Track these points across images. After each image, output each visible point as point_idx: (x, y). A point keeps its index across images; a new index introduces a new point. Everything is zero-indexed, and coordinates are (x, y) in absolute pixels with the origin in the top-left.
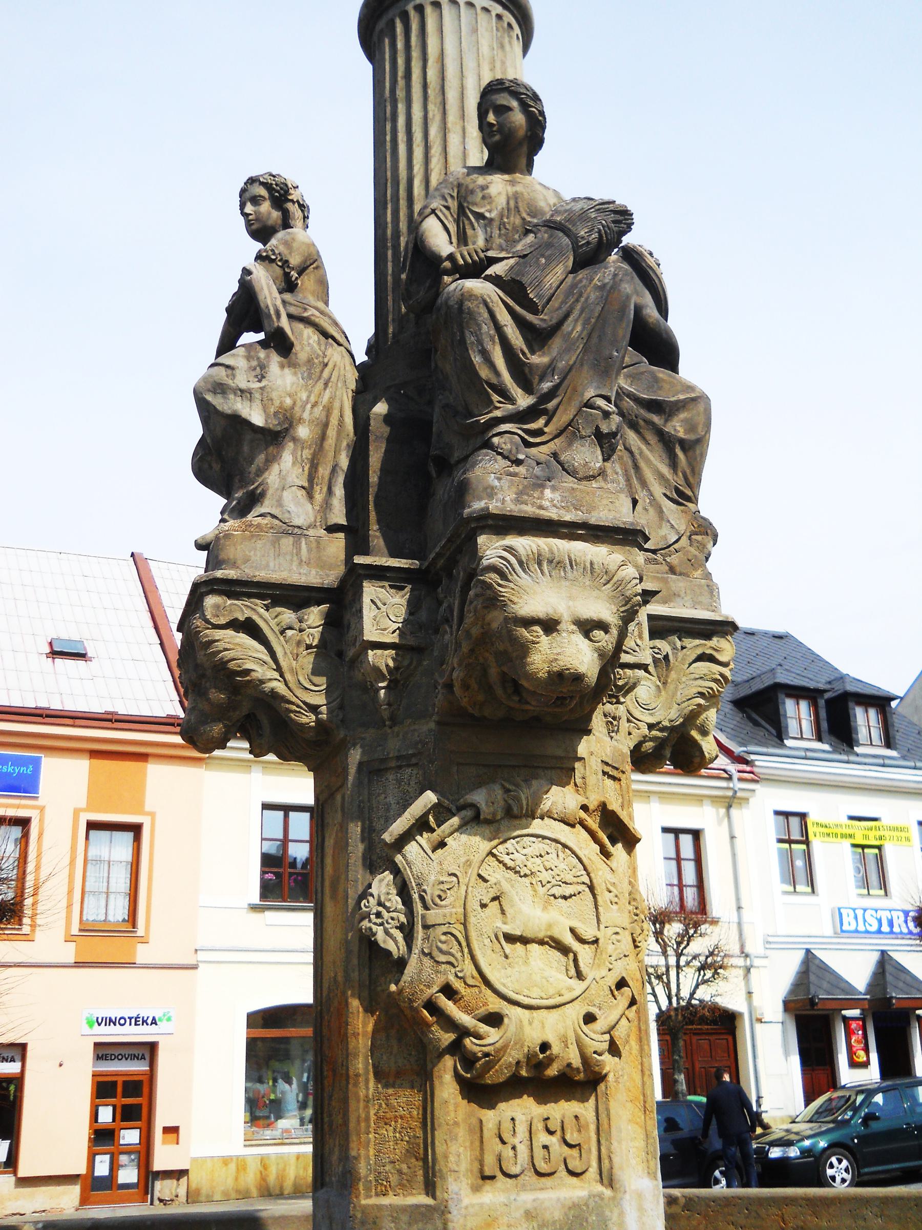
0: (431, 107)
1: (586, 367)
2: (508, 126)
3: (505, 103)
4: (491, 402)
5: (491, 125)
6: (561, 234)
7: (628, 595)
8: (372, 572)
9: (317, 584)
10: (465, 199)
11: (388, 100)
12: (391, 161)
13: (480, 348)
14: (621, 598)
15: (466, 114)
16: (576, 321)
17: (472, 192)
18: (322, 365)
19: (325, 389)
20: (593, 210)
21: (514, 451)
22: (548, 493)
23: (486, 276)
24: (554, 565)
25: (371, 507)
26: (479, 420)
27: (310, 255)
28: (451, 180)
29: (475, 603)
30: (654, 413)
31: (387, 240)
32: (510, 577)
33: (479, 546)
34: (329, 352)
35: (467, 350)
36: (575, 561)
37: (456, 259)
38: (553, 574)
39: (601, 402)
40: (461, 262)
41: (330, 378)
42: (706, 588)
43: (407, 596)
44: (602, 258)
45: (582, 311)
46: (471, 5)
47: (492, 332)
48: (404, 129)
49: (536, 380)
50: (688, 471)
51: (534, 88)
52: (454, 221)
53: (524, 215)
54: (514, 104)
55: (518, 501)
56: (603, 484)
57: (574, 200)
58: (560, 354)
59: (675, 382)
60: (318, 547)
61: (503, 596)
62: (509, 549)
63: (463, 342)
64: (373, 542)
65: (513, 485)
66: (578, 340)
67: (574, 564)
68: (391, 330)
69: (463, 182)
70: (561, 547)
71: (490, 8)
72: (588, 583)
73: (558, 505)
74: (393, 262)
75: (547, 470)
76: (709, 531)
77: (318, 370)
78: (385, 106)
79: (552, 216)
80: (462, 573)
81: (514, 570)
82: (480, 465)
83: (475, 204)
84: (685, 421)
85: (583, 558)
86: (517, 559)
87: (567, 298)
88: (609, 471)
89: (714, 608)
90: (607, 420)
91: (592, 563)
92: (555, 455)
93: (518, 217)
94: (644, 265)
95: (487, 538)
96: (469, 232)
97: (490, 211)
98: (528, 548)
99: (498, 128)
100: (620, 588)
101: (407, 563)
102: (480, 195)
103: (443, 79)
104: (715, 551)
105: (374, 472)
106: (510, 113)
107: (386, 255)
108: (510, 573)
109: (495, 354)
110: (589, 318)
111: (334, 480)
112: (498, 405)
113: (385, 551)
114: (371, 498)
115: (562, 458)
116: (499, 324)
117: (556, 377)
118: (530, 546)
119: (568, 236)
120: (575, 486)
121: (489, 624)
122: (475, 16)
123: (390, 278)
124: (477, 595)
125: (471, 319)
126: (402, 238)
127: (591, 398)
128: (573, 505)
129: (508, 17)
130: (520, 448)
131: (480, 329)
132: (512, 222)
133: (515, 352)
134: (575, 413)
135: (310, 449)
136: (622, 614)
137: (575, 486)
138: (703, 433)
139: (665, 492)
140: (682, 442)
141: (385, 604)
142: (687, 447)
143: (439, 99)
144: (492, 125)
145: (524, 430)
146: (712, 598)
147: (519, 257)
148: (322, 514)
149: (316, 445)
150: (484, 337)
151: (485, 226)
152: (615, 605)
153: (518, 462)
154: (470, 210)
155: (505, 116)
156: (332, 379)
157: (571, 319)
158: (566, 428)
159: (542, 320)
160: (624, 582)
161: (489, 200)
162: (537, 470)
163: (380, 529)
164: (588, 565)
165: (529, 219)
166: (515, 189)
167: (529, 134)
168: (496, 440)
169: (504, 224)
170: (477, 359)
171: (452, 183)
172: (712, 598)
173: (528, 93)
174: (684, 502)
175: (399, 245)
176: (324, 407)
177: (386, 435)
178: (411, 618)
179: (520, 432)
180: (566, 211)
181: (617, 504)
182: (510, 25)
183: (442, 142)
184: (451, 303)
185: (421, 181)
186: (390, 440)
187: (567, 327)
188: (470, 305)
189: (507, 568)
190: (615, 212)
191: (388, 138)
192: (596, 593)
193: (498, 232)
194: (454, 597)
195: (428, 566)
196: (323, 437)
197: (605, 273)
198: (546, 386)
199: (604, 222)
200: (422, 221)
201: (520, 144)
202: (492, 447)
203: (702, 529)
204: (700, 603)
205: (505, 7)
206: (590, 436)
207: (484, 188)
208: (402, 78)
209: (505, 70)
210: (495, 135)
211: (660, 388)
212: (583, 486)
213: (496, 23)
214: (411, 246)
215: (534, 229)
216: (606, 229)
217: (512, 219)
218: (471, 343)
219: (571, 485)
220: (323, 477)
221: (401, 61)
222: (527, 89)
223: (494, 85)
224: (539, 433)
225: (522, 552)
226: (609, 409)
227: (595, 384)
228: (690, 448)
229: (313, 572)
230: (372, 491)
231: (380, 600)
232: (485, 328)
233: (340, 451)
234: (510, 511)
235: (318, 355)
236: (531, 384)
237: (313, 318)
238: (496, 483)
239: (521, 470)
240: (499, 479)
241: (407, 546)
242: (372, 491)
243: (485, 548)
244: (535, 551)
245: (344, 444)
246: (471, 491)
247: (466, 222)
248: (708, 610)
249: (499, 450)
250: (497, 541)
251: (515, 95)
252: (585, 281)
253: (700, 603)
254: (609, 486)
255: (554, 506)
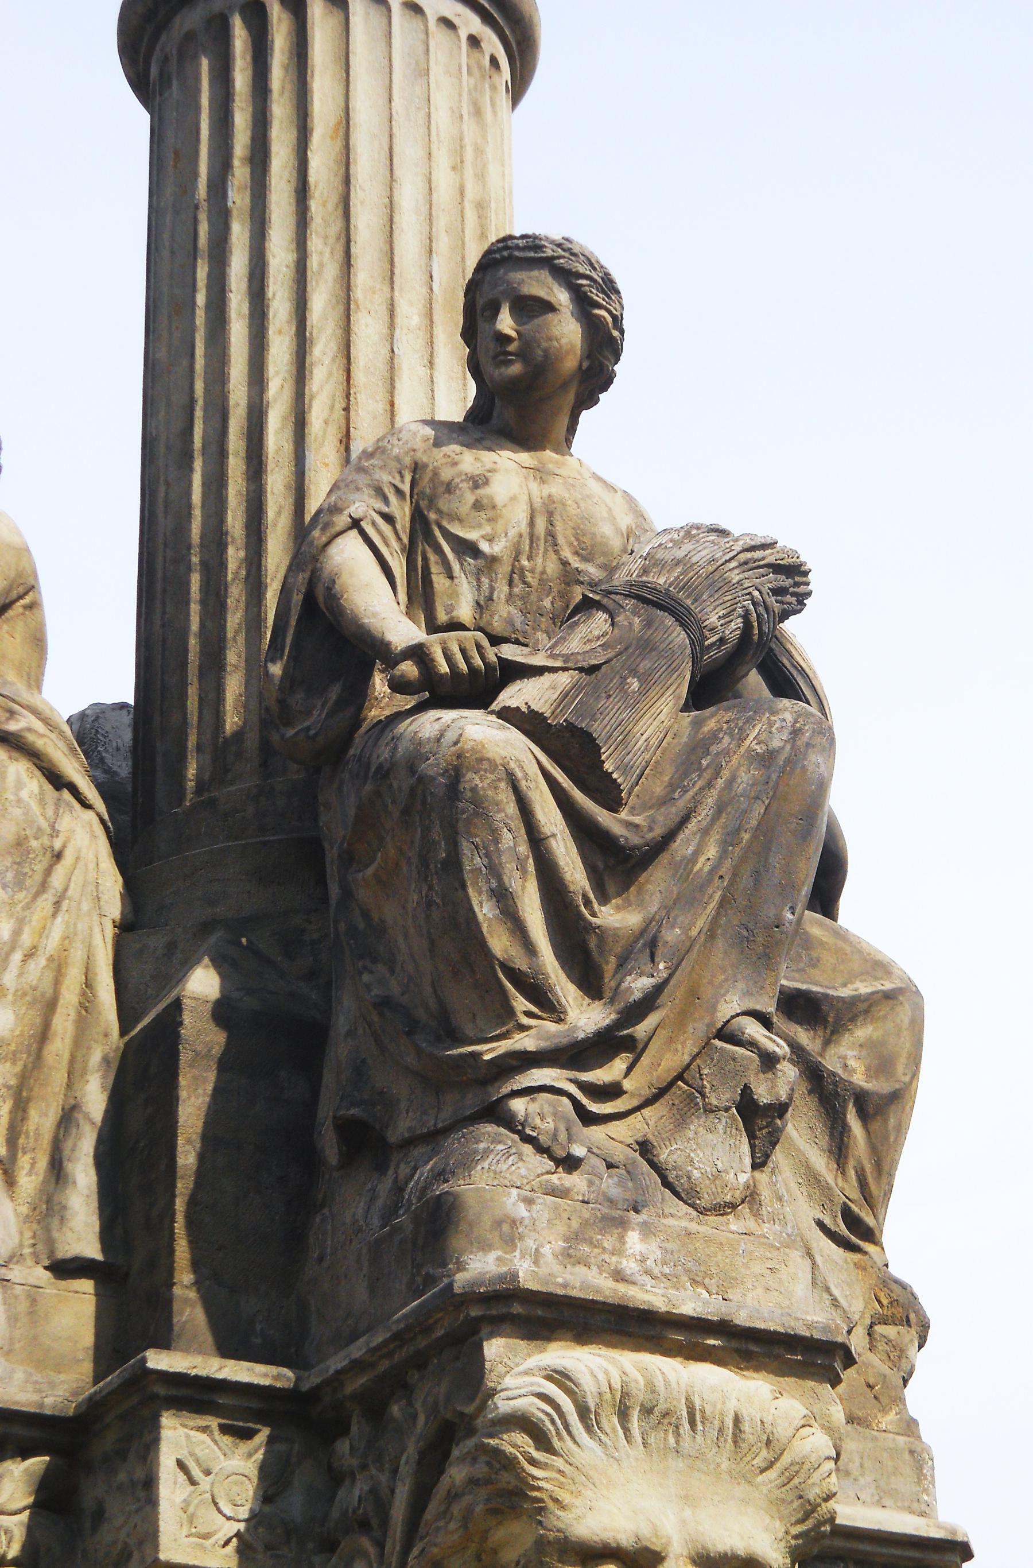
0: (315, 244)
1: (720, 943)
2: (544, 344)
3: (542, 293)
4: (511, 1012)
5: (503, 339)
6: (669, 621)
7: (812, 1499)
8: (183, 1392)
9: (29, 1404)
10: (432, 501)
11: (204, 206)
12: (207, 356)
13: (494, 884)
14: (796, 1504)
15: (397, 271)
16: (706, 832)
17: (449, 488)
18: (49, 854)
19: (54, 915)
20: (734, 564)
21: (563, 1137)
22: (633, 1239)
23: (506, 709)
24: (654, 1418)
25: (179, 1226)
26: (481, 1054)
27: (20, 574)
28: (396, 451)
29: (467, 1499)
30: (800, 1024)
31: (189, 547)
32: (557, 1444)
33: (487, 1365)
34: (65, 823)
35: (464, 887)
36: (703, 1412)
37: (433, 660)
38: (651, 1440)
39: (753, 1029)
40: (444, 668)
41: (66, 890)
42: (907, 1456)
43: (259, 1456)
44: (743, 673)
45: (720, 809)
46: (417, 10)
47: (523, 849)
48: (244, 285)
49: (610, 966)
50: (868, 1168)
51: (603, 262)
52: (403, 550)
53: (567, 554)
54: (562, 297)
55: (568, 1257)
56: (751, 1224)
57: (689, 532)
58: (668, 909)
59: (848, 949)
60: (32, 1313)
61: (539, 1489)
62: (560, 1377)
63: (453, 865)
64: (181, 1314)
65: (559, 1216)
66: (710, 881)
67: (698, 1418)
68: (192, 771)
69: (425, 459)
70: (672, 1377)
71: (456, 21)
72: (725, 1465)
73: (656, 1271)
74: (203, 602)
75: (630, 1184)
76: (912, 1316)
77: (39, 868)
78: (196, 221)
79: (645, 571)
80: (421, 1419)
81: (567, 1426)
82: (486, 1165)
83: (459, 520)
84: (868, 1046)
85: (719, 1406)
86: (575, 1402)
87: (686, 774)
88: (765, 1194)
89: (924, 1507)
90: (770, 1075)
91: (737, 1420)
92: (645, 1148)
93: (554, 557)
94: (785, 661)
95: (507, 1346)
96: (439, 581)
97: (491, 540)
98: (601, 1376)
99: (520, 348)
100: (796, 1481)
101: (266, 1375)
102: (470, 498)
103: (347, 181)
104: (923, 1360)
105: (189, 1141)
106: (550, 316)
107: (188, 584)
108: (558, 1433)
109: (526, 900)
110: (738, 830)
111: (69, 1144)
112: (525, 1021)
113: (206, 1337)
114: (180, 1205)
115: (664, 1155)
116: (539, 832)
117: (661, 966)
118: (606, 1372)
119: (684, 625)
120: (694, 1227)
121: (495, 1552)
122: (422, 36)
123: (193, 642)
124: (473, 1482)
125: (476, 814)
126: (231, 551)
127: (733, 1017)
128: (688, 1271)
129: (492, 43)
130: (574, 1130)
131: (497, 841)
132: (539, 568)
133: (572, 900)
134: (696, 1050)
135: (14, 1063)
136: (793, 1542)
137: (694, 1227)
138: (907, 1079)
139: (820, 1216)
140: (861, 1099)
141: (208, 1473)
142: (871, 1111)
143: (336, 227)
144: (507, 339)
145: (582, 1086)
146: (919, 1482)
147: (581, 670)
148: (35, 1226)
149: (29, 1055)
150: (504, 859)
151: (478, 574)
152: (781, 1519)
153: (570, 1164)
154: (441, 528)
155: (538, 321)
156: (70, 893)
157: (692, 826)
158: (671, 1084)
159: (628, 825)
160: (806, 1467)
161: (490, 513)
162: (609, 1184)
163: (197, 1283)
164: (729, 1423)
165: (575, 563)
166: (547, 490)
167: (585, 365)
168: (518, 1106)
169: (522, 570)
170: (485, 910)
171: (398, 459)
172: (919, 1482)
173: (594, 275)
174: (861, 1243)
175: (223, 565)
176: (51, 959)
177: (217, 1051)
178: (267, 1509)
179: (573, 1089)
180: (678, 563)
181: (784, 1274)
182: (494, 61)
183: (339, 332)
184: (429, 768)
185: (284, 418)
186: (224, 1065)
187: (683, 846)
188: (477, 781)
189: (553, 1422)
190: (777, 568)
191: (201, 298)
192: (740, 1490)
193: (506, 588)
194: (395, 1471)
195: (318, 1388)
196: (44, 1035)
197: (771, 724)
198: (638, 985)
199: (756, 593)
200: (328, 543)
201: (564, 386)
202: (509, 1122)
203: (899, 1312)
204: (892, 1493)
205: (487, 18)
206: (727, 1109)
207: (478, 482)
208: (243, 160)
209: (484, 166)
210: (511, 362)
211: (814, 963)
212: (707, 1227)
213: (468, 56)
214: (297, 599)
215: (605, 601)
216: (761, 609)
217: (539, 560)
218: (472, 871)
219: (684, 1223)
220: (38, 1135)
221: (241, 120)
222: (591, 264)
223: (517, 247)
224: (611, 1091)
225: (588, 1386)
226: (777, 1049)
227: (741, 985)
228: (876, 1114)
229: (19, 1375)
230: (183, 1187)
231: (197, 1461)
232: (507, 838)
233: (84, 1072)
234: (565, 1286)
235: (39, 829)
236: (600, 977)
237: (31, 738)
238: (522, 1211)
239: (576, 1181)
240: (529, 1202)
241: (258, 1327)
242: (183, 1187)
243: (501, 1369)
244: (617, 1385)
245: (96, 1057)
246: (463, 1226)
247: (432, 558)
248: (912, 1512)
249: (528, 1131)
250: (529, 1356)
251: (566, 277)
252: (727, 740)
253: (892, 1493)
254: (766, 1228)
255: (648, 1272)
